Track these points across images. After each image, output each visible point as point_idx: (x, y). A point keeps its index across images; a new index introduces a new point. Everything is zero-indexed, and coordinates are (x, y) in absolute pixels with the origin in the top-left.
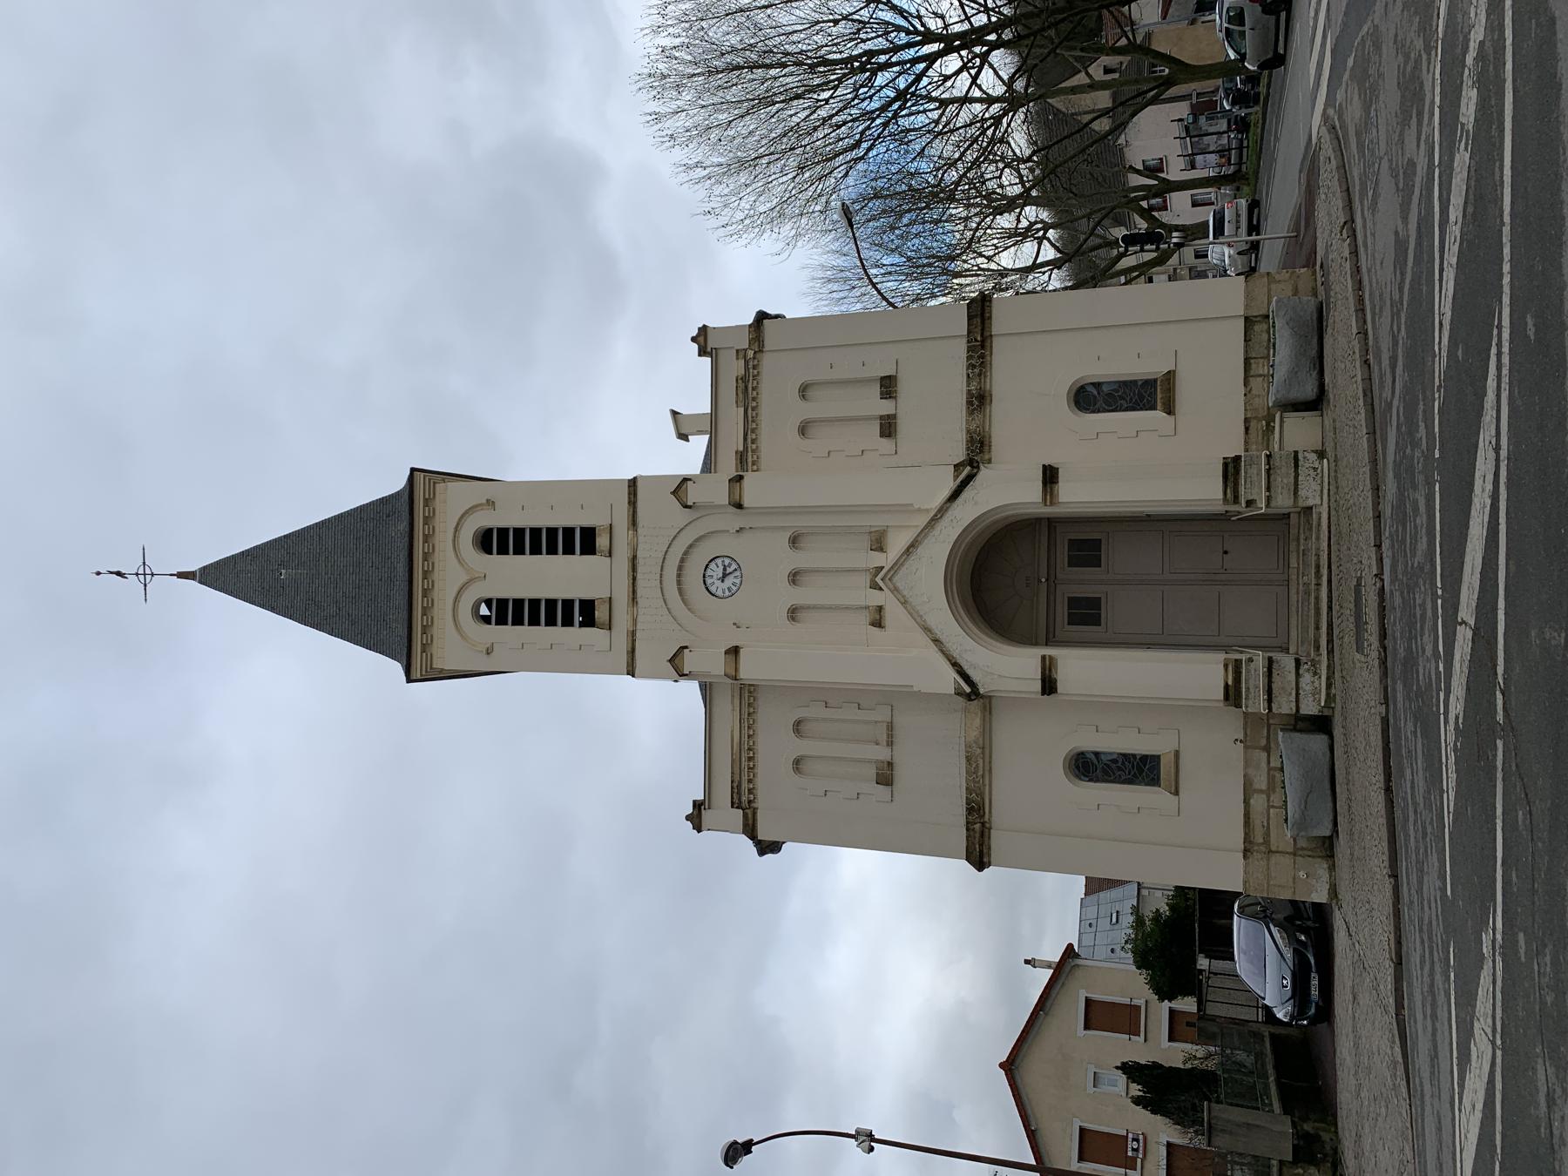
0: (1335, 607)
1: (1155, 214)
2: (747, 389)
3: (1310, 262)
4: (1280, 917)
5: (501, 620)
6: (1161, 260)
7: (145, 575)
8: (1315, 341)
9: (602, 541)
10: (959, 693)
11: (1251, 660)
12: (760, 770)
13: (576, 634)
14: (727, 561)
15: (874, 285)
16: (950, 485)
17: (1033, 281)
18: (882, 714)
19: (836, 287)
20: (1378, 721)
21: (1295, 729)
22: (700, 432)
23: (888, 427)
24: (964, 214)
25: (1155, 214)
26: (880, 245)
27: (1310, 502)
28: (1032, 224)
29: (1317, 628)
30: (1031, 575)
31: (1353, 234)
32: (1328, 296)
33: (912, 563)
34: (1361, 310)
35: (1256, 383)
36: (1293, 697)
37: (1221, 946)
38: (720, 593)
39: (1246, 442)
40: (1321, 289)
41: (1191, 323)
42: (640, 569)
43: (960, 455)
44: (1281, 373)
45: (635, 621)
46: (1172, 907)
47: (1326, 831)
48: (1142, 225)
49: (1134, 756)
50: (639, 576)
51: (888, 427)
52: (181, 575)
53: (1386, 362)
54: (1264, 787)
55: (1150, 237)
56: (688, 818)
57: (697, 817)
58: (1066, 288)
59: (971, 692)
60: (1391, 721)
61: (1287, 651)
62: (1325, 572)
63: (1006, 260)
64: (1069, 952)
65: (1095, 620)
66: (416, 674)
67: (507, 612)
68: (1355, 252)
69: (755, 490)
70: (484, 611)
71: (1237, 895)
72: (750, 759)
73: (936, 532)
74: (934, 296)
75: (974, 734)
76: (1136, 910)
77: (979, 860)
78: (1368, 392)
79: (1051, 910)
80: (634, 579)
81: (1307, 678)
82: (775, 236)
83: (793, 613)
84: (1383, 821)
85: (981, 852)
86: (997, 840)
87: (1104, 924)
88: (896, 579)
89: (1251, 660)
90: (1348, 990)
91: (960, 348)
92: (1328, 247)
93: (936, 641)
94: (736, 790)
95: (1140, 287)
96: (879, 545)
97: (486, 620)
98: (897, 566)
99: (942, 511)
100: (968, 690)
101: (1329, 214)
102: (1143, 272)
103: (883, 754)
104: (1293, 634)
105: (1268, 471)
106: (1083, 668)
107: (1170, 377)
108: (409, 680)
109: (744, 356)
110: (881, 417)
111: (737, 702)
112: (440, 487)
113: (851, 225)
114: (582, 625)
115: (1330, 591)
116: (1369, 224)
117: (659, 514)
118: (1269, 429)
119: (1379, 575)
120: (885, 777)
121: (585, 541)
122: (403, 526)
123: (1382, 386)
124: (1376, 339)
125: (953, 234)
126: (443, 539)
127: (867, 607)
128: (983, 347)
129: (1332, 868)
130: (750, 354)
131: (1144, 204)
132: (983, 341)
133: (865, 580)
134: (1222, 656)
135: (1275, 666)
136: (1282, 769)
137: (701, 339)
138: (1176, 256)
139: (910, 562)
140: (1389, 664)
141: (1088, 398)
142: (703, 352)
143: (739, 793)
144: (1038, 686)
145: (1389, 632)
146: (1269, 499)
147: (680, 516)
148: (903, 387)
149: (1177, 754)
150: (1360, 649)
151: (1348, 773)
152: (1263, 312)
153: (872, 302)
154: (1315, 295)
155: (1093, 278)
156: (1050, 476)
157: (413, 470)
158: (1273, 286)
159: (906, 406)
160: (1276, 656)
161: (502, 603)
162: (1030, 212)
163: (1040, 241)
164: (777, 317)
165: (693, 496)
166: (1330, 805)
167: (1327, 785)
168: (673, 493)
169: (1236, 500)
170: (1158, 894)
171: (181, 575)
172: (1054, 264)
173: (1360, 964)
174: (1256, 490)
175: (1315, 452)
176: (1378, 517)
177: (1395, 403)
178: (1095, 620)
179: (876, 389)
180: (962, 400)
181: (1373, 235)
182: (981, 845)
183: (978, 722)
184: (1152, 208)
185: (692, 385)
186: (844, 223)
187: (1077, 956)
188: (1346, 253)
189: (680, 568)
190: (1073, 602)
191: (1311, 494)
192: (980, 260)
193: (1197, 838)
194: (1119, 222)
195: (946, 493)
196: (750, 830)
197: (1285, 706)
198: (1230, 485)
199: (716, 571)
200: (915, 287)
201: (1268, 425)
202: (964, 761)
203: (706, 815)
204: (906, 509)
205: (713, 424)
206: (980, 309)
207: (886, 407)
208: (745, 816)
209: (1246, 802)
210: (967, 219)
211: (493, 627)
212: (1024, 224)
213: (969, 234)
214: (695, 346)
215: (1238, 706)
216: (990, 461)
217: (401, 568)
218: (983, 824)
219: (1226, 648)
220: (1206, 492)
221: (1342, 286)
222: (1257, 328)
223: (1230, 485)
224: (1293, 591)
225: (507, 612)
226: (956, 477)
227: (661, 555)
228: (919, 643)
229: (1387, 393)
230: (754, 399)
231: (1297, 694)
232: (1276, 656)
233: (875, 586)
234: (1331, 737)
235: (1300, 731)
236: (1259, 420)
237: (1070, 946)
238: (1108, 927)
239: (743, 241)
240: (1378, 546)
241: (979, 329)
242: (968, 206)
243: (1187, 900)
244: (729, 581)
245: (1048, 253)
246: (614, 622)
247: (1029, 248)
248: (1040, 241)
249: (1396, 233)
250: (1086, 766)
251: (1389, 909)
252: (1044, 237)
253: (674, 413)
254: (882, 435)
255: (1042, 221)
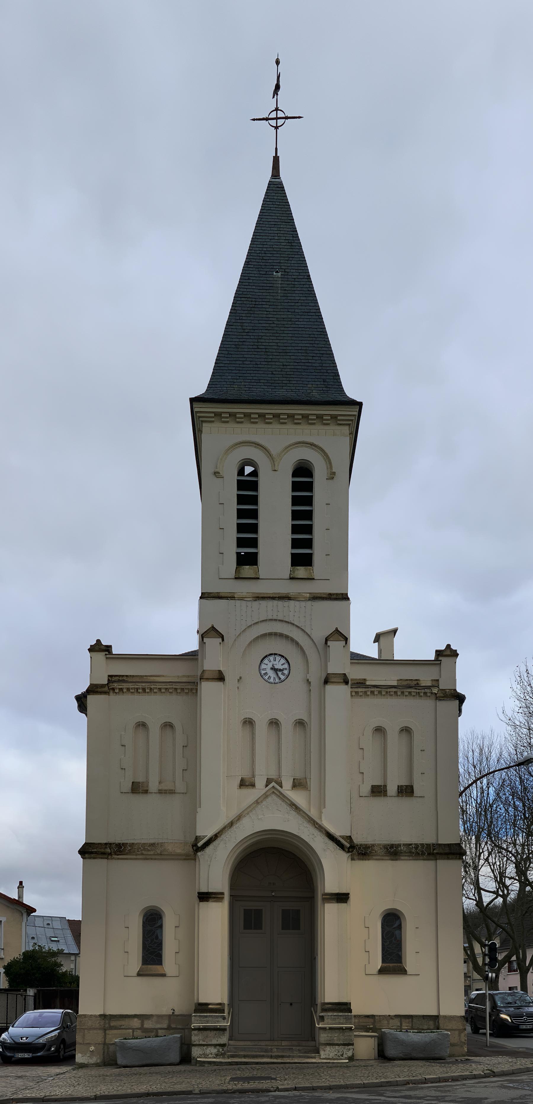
0: (258, 1066)
1: (507, 965)
2: (410, 688)
3: (470, 1053)
4: (65, 1036)
5: (241, 485)
6: (476, 968)
7: (277, 119)
8: (422, 1056)
9: (301, 571)
10: (197, 839)
11: (224, 1018)
12: (136, 697)
13: (231, 550)
14: (286, 672)
15: (475, 782)
16: (337, 832)
17: (469, 889)
18: (180, 787)
19: (476, 754)
20: (189, 1089)
21: (182, 1044)
22: (380, 651)
23: (378, 791)
24: (518, 842)
25: (507, 965)
26: (503, 785)
27: (322, 1053)
28: (507, 888)
29: (245, 1056)
30: (277, 887)
31: (486, 1076)
32: (449, 1063)
33: (285, 807)
34: (439, 1080)
35: (396, 1022)
36: (201, 1042)
37: (43, 1002)
38: (263, 666)
39: (360, 1016)
40: (453, 1059)
41: (436, 984)
42: (280, 603)
43: (358, 840)
44: (401, 1036)
45: (241, 599)
46: (65, 974)
47: (120, 1061)
48: (500, 957)
49: (161, 949)
50: (275, 602)
51: (378, 791)
52: (276, 160)
53: (411, 1093)
54: (146, 1026)
55: (493, 960)
56: (98, 641)
57: (99, 648)
58: (463, 910)
59: (198, 847)
60: (190, 1096)
61: (231, 1039)
62: (279, 1061)
63: (485, 871)
64: (31, 910)
65: (247, 926)
66: (199, 407)
67: (248, 489)
68: (475, 1077)
69: (338, 693)
70: (248, 470)
71: (77, 1012)
72: (144, 690)
73: (306, 824)
74: (464, 823)
75: (170, 848)
76: (60, 952)
77: (85, 851)
78: (389, 1084)
79: (59, 899)
80: (273, 598)
81: (214, 1050)
82: (517, 709)
83: (249, 722)
84: (129, 1091)
85: (92, 853)
86: (100, 864)
87: (50, 933)
88: (274, 797)
89: (224, 1018)
90: (23, 1074)
91: (429, 839)
92: (479, 1063)
93: (231, 824)
94: (121, 679)
95: (461, 955)
96: (298, 784)
97: (241, 472)
98: (283, 797)
99: (320, 828)
100: (200, 844)
101: (499, 1063)
102: (470, 957)
103: (153, 786)
104: (241, 1043)
105: (341, 1028)
106: (216, 918)
107: (403, 971)
108: (192, 400)
109: (432, 687)
110: (385, 786)
111: (184, 680)
112: (346, 430)
113: (519, 765)
114: (238, 554)
115: (267, 1063)
116: (492, 1084)
117: (319, 619)
118: (367, 1030)
119: (278, 1089)
120: (138, 788)
121: (302, 560)
122: (316, 395)
123: (392, 1091)
124: (422, 1088)
125: (505, 838)
126: (247, 432)
127: (253, 776)
128: (429, 854)
129: (97, 1065)
130: (435, 690)
131: (514, 958)
132: (433, 854)
133: (273, 775)
134: (226, 1001)
135: (222, 1032)
136: (157, 1036)
137: (448, 652)
138: (479, 977)
139: (285, 806)
140: (224, 1095)
141: (392, 923)
142: (439, 653)
143: (119, 681)
144: (204, 890)
145: (244, 1095)
146: (324, 1029)
147: (320, 634)
148: (405, 802)
149: (164, 975)
150: (232, 1079)
151: (157, 1073)
152: (441, 1026)
153: (464, 781)
154: (450, 1056)
155: (468, 926)
156: (342, 898)
157: (360, 404)
158: (457, 1032)
159: (391, 804)
160: (227, 1034)
161: (254, 486)
162: (516, 886)
163: (496, 893)
164: (460, 711)
165: (335, 645)
166: (137, 1064)
167: (148, 1062)
168: (337, 630)
169: (324, 1010)
170: (72, 966)
171: (276, 160)
172: (479, 902)
173: (40, 1080)
174: (330, 1021)
175: (353, 1055)
176: (314, 1089)
177: (383, 1098)
178: (247, 926)
179: (404, 782)
180: (395, 841)
181: (486, 1086)
182: (96, 853)
183: (178, 851)
184: (510, 963)
185: (414, 646)
186: (521, 759)
187: (29, 915)
188: (475, 1073)
189: (281, 635)
190: (259, 913)
191: (327, 1053)
192: (486, 853)
193: (112, 988)
194: (502, 943)
195: (332, 830)
196: (93, 689)
197: (196, 1038)
198: (334, 1007)
199: (280, 663)
200: (471, 810)
201: (370, 1029)
202: (152, 841)
203: (101, 656)
204: (322, 803)
205: (385, 661)
206: (455, 852)
207: (392, 789)
208: (103, 686)
209: (135, 1016)
210: (515, 844)
211: (235, 478)
212: (508, 882)
213: (505, 846)
214: (443, 647)
215: (196, 1011)
216: (352, 859)
217: (281, 393)
218: (110, 854)
219: (231, 1004)
220: (330, 992)
221: (456, 1071)
222: (431, 1023)
223: (334, 1007)
224: (267, 1043)
225: (248, 489)
226: (342, 837)
227: (291, 620)
228: (231, 811)
229: (389, 1094)
230: (403, 693)
231: (204, 1045)
232: (227, 1034)
233: (269, 782)
234: (178, 1064)
235: (181, 1047)
236: (373, 1024)
237: (34, 910)
238: (48, 935)
239: (515, 686)
240: (296, 1089)
241: (441, 851)
242: (523, 845)
243: (70, 983)
244: (271, 674)
245: (487, 898)
246: (294, 581)
247: (492, 886)
248: (496, 893)
249: (486, 1099)
250: (152, 921)
251: (76, 1095)
252: (498, 895)
253: (395, 631)
254: (373, 787)
255: (508, 894)
